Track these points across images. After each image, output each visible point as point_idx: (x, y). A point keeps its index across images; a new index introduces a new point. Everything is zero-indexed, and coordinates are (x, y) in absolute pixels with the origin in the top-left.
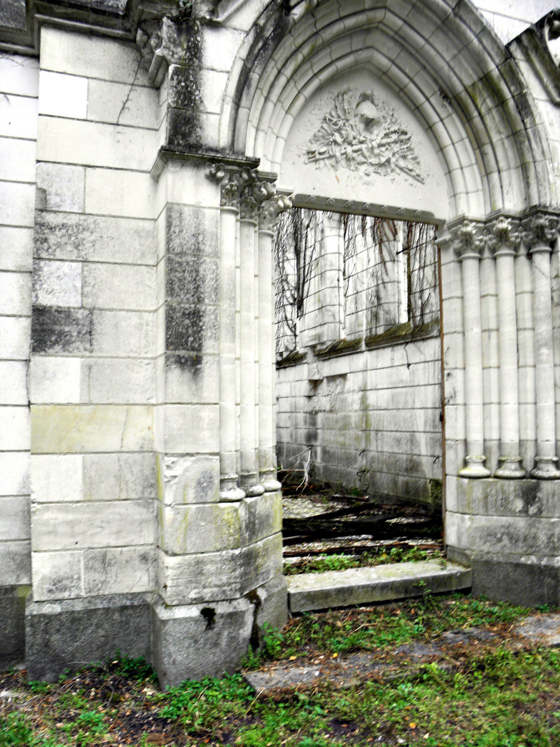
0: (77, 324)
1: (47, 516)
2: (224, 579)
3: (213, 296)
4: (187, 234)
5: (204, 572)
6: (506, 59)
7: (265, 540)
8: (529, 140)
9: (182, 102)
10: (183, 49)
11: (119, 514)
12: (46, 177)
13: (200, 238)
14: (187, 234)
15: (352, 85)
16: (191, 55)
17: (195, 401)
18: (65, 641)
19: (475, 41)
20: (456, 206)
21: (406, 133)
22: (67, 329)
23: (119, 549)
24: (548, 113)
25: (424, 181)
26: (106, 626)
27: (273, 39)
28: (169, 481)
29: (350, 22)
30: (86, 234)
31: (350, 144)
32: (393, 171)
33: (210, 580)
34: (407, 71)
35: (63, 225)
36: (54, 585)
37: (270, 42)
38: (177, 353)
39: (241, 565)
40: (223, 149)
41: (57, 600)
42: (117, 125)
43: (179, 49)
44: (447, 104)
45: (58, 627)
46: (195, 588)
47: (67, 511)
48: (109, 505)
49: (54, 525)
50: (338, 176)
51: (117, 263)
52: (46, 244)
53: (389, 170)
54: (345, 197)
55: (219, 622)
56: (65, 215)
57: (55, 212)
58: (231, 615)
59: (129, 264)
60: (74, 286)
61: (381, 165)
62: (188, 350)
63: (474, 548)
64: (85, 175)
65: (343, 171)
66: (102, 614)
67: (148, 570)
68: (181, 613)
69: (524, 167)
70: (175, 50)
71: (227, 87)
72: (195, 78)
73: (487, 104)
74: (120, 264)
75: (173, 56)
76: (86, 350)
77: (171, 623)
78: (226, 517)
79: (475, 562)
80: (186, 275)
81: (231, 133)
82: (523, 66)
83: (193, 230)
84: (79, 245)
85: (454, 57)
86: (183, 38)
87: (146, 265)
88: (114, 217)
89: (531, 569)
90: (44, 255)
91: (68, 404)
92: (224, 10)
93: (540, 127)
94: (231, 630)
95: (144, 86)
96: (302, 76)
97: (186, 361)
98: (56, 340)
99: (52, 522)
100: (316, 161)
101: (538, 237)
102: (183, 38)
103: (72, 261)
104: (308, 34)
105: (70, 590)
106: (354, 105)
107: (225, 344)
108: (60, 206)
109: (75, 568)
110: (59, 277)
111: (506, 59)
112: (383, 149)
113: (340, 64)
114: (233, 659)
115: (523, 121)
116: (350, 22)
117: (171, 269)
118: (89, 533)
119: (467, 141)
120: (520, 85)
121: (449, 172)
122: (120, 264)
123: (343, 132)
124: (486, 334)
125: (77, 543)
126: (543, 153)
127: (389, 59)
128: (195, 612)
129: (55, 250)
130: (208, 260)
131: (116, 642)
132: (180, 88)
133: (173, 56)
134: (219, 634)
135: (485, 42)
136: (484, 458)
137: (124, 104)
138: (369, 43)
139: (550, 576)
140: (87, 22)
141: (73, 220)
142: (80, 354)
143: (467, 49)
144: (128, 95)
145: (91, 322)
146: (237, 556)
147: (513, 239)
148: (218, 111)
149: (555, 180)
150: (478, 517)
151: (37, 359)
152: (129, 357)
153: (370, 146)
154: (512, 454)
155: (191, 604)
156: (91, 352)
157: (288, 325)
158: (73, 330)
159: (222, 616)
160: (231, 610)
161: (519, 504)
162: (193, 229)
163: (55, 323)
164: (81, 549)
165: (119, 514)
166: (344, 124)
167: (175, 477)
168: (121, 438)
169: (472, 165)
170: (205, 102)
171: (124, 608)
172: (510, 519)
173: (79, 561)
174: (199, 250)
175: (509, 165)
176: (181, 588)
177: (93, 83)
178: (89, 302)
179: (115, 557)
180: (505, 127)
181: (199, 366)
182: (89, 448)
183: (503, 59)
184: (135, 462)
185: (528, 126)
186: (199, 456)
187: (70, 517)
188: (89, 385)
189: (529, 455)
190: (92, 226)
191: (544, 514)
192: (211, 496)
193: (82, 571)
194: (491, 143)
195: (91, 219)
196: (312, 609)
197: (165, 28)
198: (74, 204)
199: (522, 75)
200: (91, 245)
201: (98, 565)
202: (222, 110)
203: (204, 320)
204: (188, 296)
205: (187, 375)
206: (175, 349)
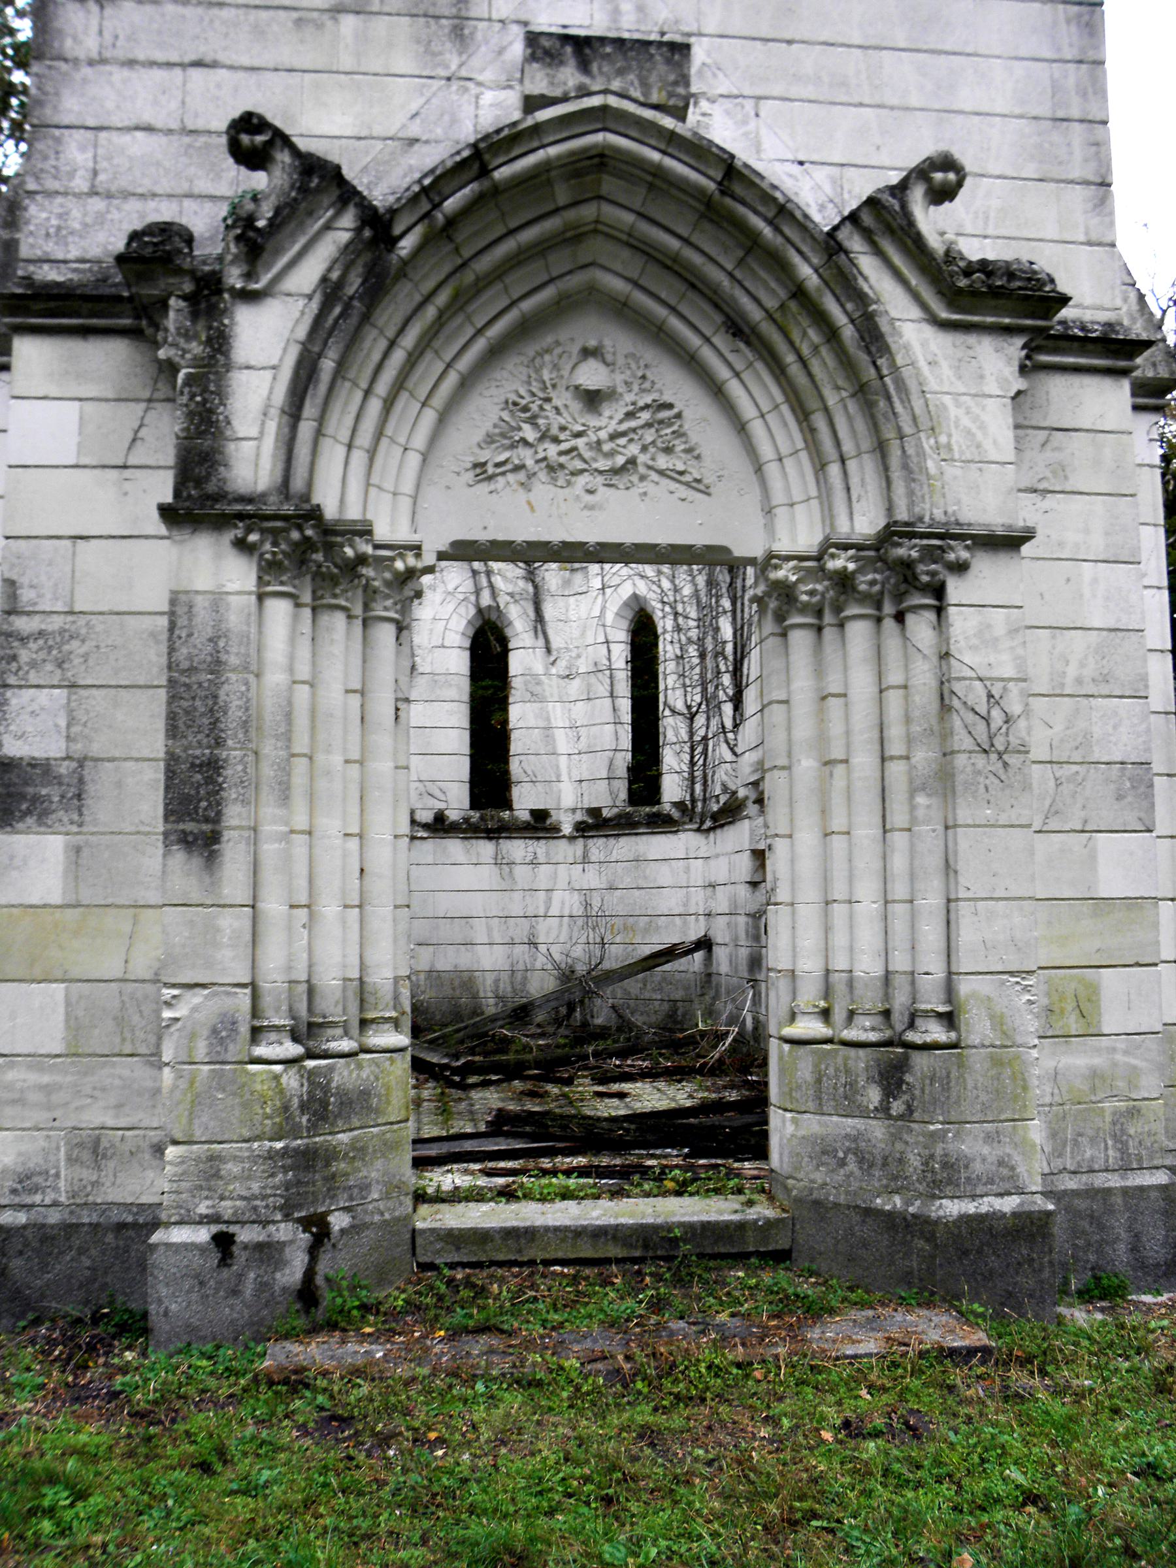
2: (256, 1187)
3: (241, 736)
4: (199, 639)
6: (830, 256)
7: (356, 1133)
8: (889, 398)
9: (197, 428)
10: (200, 343)
11: (120, 1077)
12: (16, 561)
13: (221, 644)
14: (199, 639)
15: (563, 334)
16: (214, 350)
17: (209, 902)
18: (30, 1270)
19: (767, 231)
20: (770, 529)
21: (670, 406)
22: (44, 792)
24: (924, 344)
25: (711, 490)
26: (93, 1252)
27: (361, 299)
28: (168, 1026)
29: (528, 235)
30: (75, 644)
31: (556, 440)
32: (643, 478)
33: (231, 1187)
34: (663, 295)
36: (20, 1182)
37: (356, 303)
38: (181, 826)
39: (285, 1169)
40: (263, 496)
41: (24, 1206)
42: (125, 467)
43: (194, 344)
44: (742, 345)
45: (20, 1247)
46: (207, 1198)
47: (41, 1069)
48: (105, 1063)
49: (22, 1091)
52: (14, 664)
53: (635, 478)
54: (545, 537)
55: (240, 1257)
56: (43, 616)
57: (28, 613)
58: (260, 1247)
59: (140, 687)
60: (56, 726)
61: (616, 471)
62: (198, 821)
63: (800, 1175)
65: (542, 490)
66: (87, 1233)
68: (180, 1235)
69: (881, 449)
70: (186, 346)
71: (271, 392)
72: (219, 386)
73: (810, 339)
74: (126, 687)
76: (72, 823)
77: (162, 1249)
78: (258, 1087)
79: (798, 1201)
80: (198, 703)
81: (280, 466)
82: (867, 264)
83: (209, 632)
85: (741, 263)
86: (201, 326)
88: (118, 613)
89: (892, 1222)
91: (45, 906)
92: (269, 267)
93: (906, 372)
94: (261, 1272)
96: (449, 339)
97: (196, 839)
99: (19, 1085)
100: (490, 478)
101: (906, 580)
102: (201, 326)
103: (53, 687)
104: (447, 268)
105: (43, 1193)
106: (565, 373)
107: (269, 812)
108: (35, 604)
109: (52, 1158)
111: (830, 256)
112: (622, 441)
113: (527, 305)
114: (263, 1319)
115: (874, 363)
116: (528, 235)
117: (173, 697)
118: (74, 1105)
119: (785, 408)
120: (861, 298)
121: (759, 469)
122: (126, 687)
123: (541, 421)
124: (827, 768)
126: (914, 419)
127: (628, 280)
128: (203, 1235)
130: (233, 677)
131: (109, 1279)
132: (192, 406)
133: (182, 356)
134: (240, 1276)
135: (787, 230)
136: (822, 1004)
138: (584, 258)
139: (922, 1234)
140: (79, 316)
141: (55, 624)
142: (63, 829)
143: (759, 246)
145: (81, 781)
146: (277, 1152)
147: (863, 587)
148: (254, 432)
149: (940, 468)
150: (806, 1116)
152: (138, 833)
153: (594, 439)
154: (870, 1000)
155: (200, 1223)
156: (80, 825)
157: (727, 742)
158: (51, 792)
159: (246, 1247)
160: (262, 1238)
161: (874, 1096)
162: (209, 630)
163: (26, 784)
165: (120, 1077)
166: (541, 408)
167: (177, 1020)
168: (124, 957)
169: (797, 452)
171: (121, 1226)
172: (851, 1124)
173: (58, 1148)
174: (218, 662)
175: (858, 446)
177: (89, 407)
178: (78, 748)
179: (113, 1146)
180: (848, 378)
181: (216, 847)
182: (76, 973)
183: (826, 257)
184: (146, 997)
185: (885, 372)
186: (215, 988)
187: (46, 1079)
188: (77, 877)
189: (900, 1001)
190: (83, 631)
191: (916, 1115)
192: (235, 1050)
194: (826, 409)
195: (82, 621)
196: (456, 1259)
197: (172, 314)
198: (57, 599)
199: (866, 279)
201: (86, 1155)
202: (262, 433)
203: (225, 773)
204: (199, 737)
205: (197, 862)
206: (177, 822)
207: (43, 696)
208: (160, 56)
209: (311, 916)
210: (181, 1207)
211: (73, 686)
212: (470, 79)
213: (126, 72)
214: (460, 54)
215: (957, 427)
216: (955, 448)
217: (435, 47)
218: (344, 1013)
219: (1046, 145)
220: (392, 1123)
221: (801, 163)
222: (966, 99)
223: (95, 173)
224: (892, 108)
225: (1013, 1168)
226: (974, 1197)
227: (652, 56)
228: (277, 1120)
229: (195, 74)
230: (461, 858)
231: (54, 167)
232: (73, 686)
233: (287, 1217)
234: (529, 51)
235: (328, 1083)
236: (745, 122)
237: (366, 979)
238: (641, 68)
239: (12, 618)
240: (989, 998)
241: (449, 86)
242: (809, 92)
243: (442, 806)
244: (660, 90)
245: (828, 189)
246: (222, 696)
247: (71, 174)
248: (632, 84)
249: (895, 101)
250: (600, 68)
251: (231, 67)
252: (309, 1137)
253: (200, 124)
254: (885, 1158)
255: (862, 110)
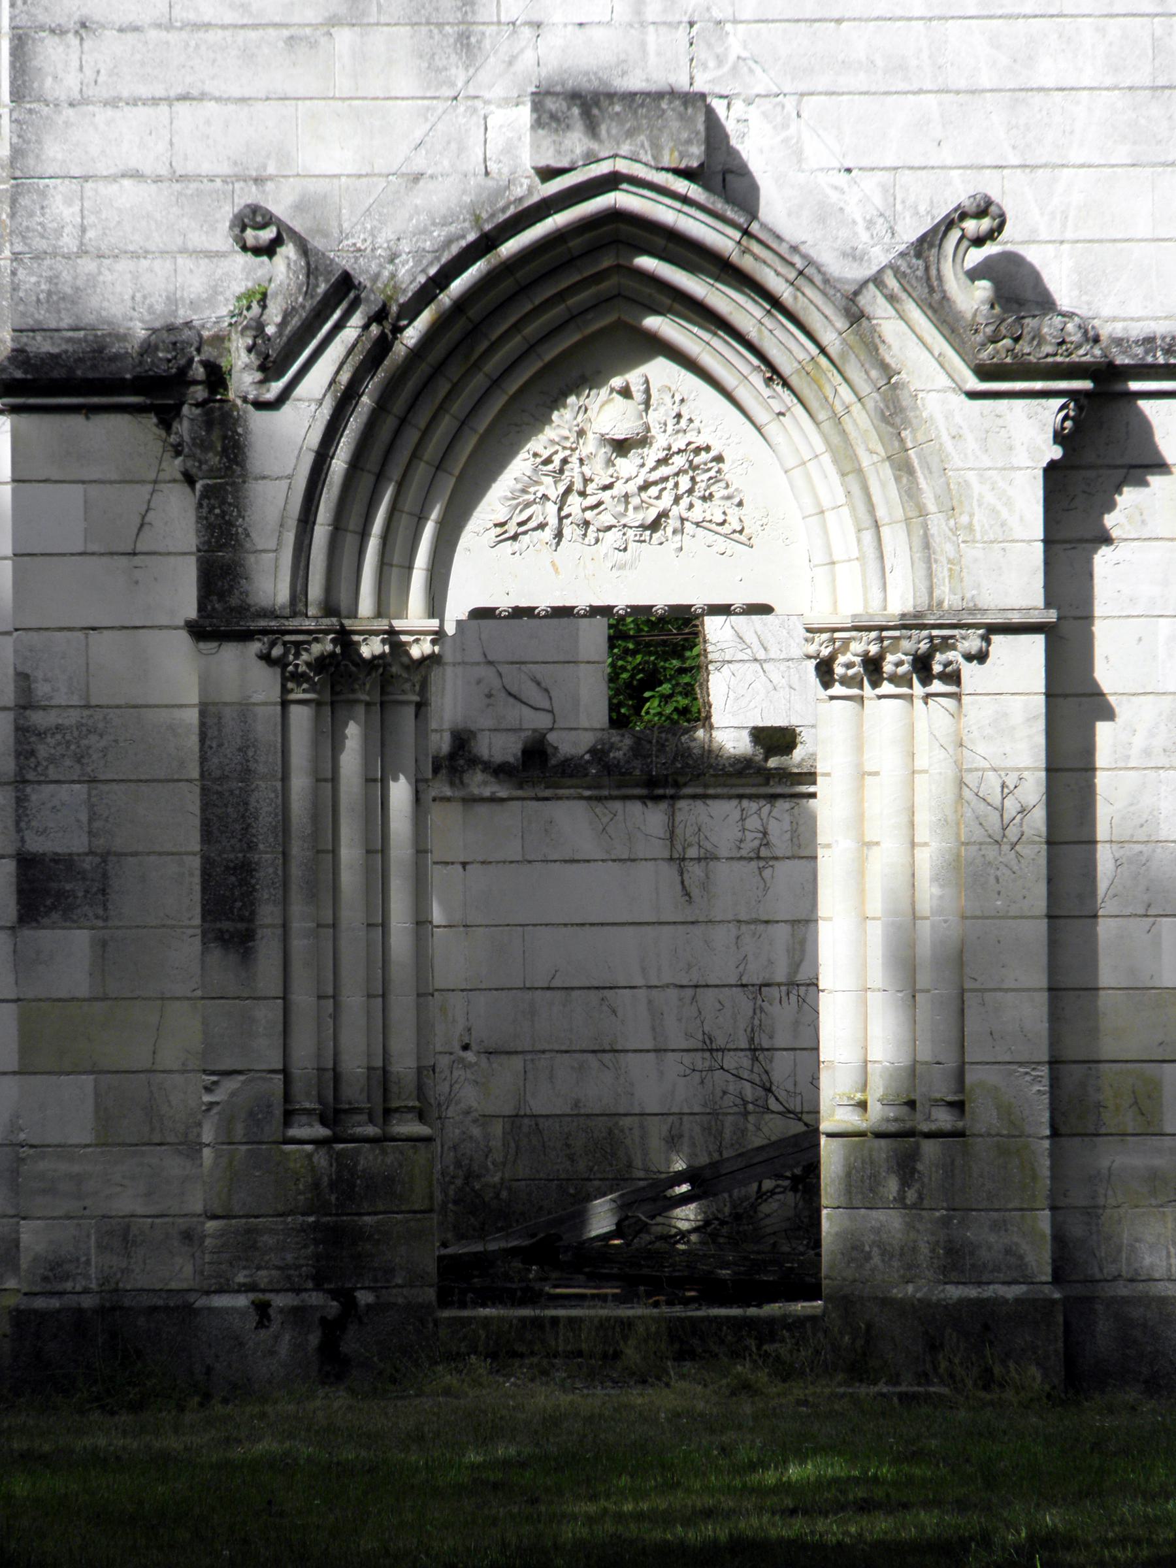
0: (84, 879)
1: (43, 1165)
2: (289, 1257)
5: (259, 1244)
7: (381, 1217)
9: (217, 542)
13: (250, 753)
16: (229, 460)
21: (708, 449)
22: (68, 887)
23: (150, 1220)
30: (93, 739)
35: (57, 728)
36: (51, 1270)
38: (218, 925)
42: (134, 554)
43: (210, 455)
46: (244, 1268)
50: (557, 563)
51: (141, 781)
52: (33, 760)
60: (78, 821)
62: (233, 920)
64: (87, 645)
67: (193, 1255)
72: (236, 498)
74: (147, 781)
75: (200, 468)
78: (292, 1165)
80: (230, 810)
84: (82, 757)
87: (187, 780)
90: (31, 776)
91: (72, 999)
95: (174, 481)
98: (53, 904)
103: (73, 782)
108: (51, 698)
110: (54, 808)
117: (207, 804)
125: (85, 1208)
129: (47, 768)
130: (262, 784)
133: (200, 468)
136: (859, 1096)
137: (144, 517)
141: (71, 718)
142: (88, 924)
144: (149, 502)
145: (105, 875)
146: (309, 1225)
148: (272, 545)
151: (27, 933)
152: (164, 926)
155: (238, 1291)
156: (106, 920)
159: (281, 1310)
161: (892, 1186)
162: (239, 741)
164: (91, 1217)
167: (217, 1103)
170: (253, 535)
171: (154, 1309)
173: (88, 1236)
174: (248, 771)
176: (223, 1267)
178: (100, 843)
181: (250, 944)
186: (252, 1074)
190: (101, 725)
191: (926, 1204)
193: (93, 1251)
198: (73, 693)
200: (101, 754)
203: (257, 875)
204: (233, 841)
207: (64, 792)
208: (144, 91)
209: (336, 1006)
210: (221, 1277)
211: (93, 781)
212: (477, 97)
213: (109, 112)
214: (467, 68)
215: (980, 506)
216: (977, 527)
217: (439, 63)
218: (369, 1100)
219: (1143, 121)
220: (415, 1212)
221: (849, 170)
222: (1047, 72)
223: (84, 230)
224: (958, 92)
225: (1021, 1258)
226: (979, 1284)
227: (664, 111)
228: (309, 1195)
229: (182, 108)
230: (588, 846)
231: (40, 224)
232: (93, 781)
233: (318, 1287)
234: (535, 116)
235: (356, 1164)
236: (785, 126)
237: (388, 1068)
238: (651, 127)
239: (28, 712)
240: (996, 1088)
241: (455, 108)
242: (859, 81)
243: (541, 721)
244: (672, 151)
245: (878, 200)
246: (253, 803)
247: (59, 233)
248: (643, 146)
249: (962, 84)
250: (608, 132)
251: (218, 100)
252: (337, 1215)
253: (190, 168)
254: (902, 1249)
255: (922, 96)
